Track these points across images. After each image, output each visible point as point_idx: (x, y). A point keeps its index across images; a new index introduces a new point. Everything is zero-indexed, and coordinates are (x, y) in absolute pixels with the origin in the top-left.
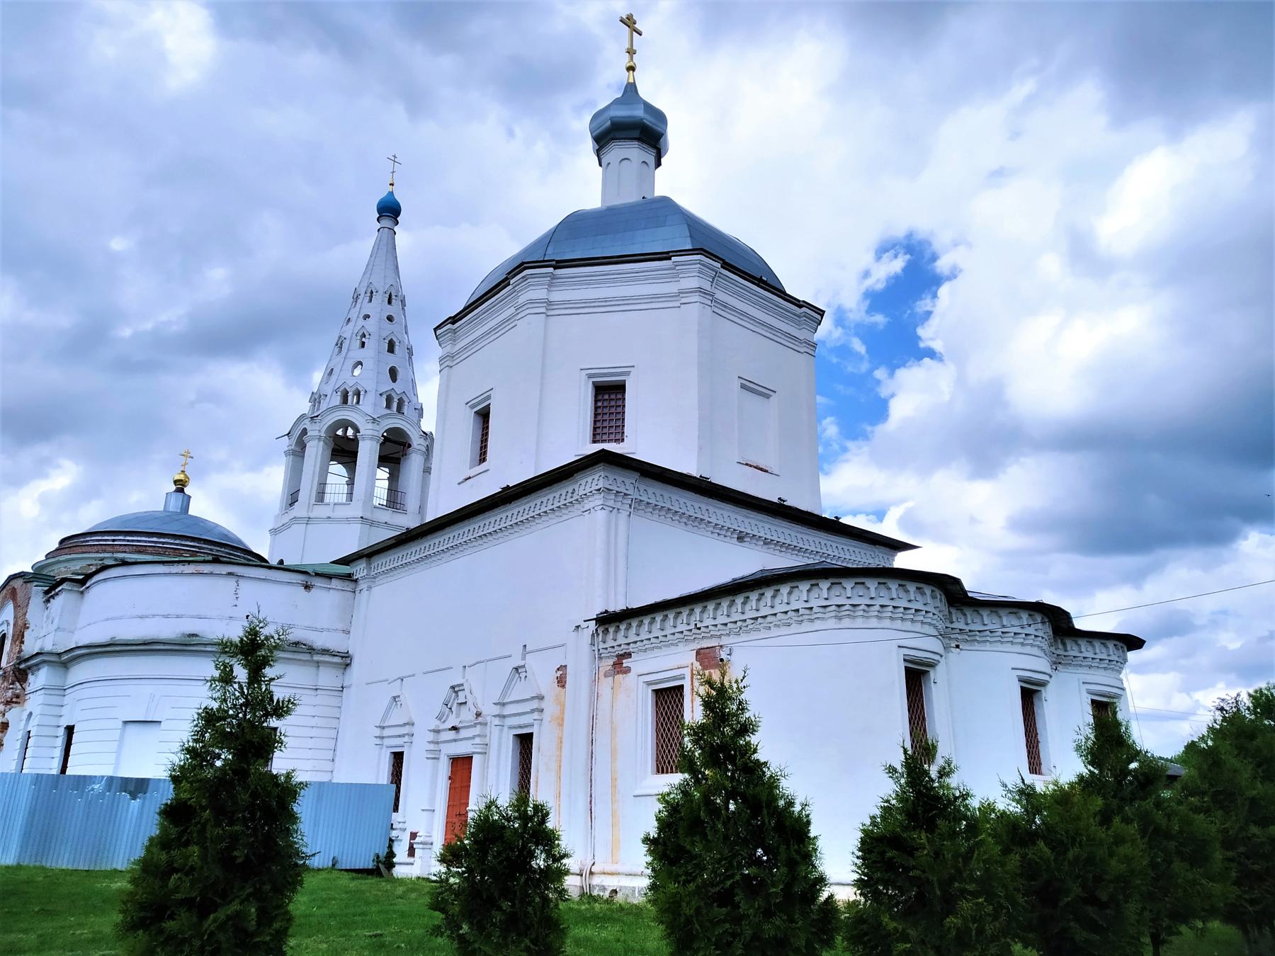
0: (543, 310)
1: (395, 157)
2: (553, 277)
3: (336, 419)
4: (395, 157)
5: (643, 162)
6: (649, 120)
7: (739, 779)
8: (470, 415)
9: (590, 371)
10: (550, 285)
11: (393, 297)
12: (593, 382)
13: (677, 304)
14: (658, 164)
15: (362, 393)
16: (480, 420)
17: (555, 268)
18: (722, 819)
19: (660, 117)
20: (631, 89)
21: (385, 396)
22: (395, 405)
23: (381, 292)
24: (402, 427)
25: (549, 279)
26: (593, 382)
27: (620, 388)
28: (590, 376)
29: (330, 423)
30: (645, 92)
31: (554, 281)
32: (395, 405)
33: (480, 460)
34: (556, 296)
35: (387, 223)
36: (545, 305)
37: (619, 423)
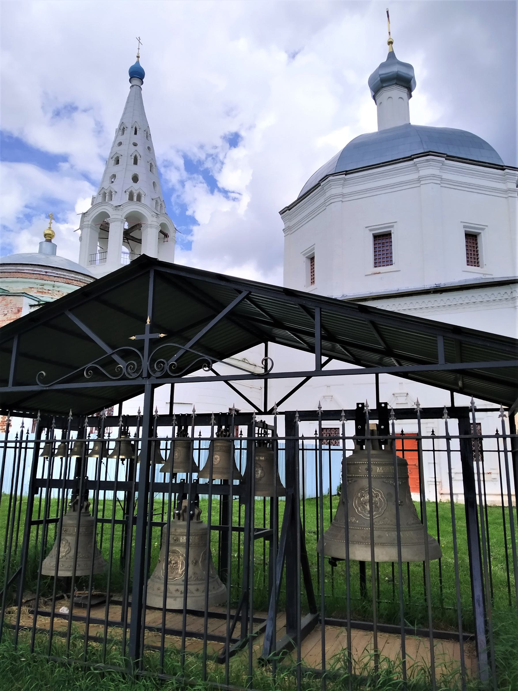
0: (439, 182)
1: (139, 38)
2: (345, 180)
3: (99, 212)
4: (139, 38)
5: (400, 98)
6: (403, 71)
7: (32, 672)
8: (304, 259)
9: (370, 228)
10: (343, 185)
11: (138, 130)
12: (373, 234)
13: (418, 185)
14: (410, 96)
15: (113, 193)
16: (309, 262)
17: (346, 175)
18: (140, 672)
19: (410, 67)
20: (391, 55)
21: (128, 193)
22: (135, 198)
23: (130, 127)
24: (167, 223)
25: (343, 181)
26: (373, 234)
27: (388, 235)
28: (371, 230)
29: (96, 215)
30: (400, 57)
31: (345, 182)
32: (135, 198)
33: (312, 282)
34: (445, 176)
35: (136, 82)
36: (341, 196)
37: (388, 252)
